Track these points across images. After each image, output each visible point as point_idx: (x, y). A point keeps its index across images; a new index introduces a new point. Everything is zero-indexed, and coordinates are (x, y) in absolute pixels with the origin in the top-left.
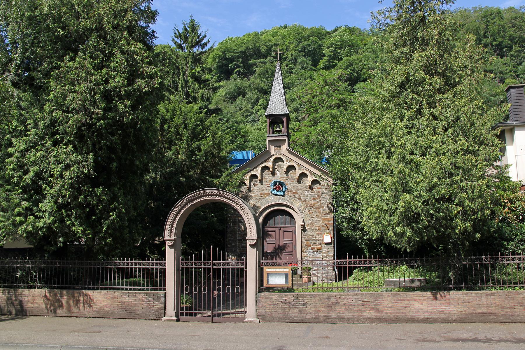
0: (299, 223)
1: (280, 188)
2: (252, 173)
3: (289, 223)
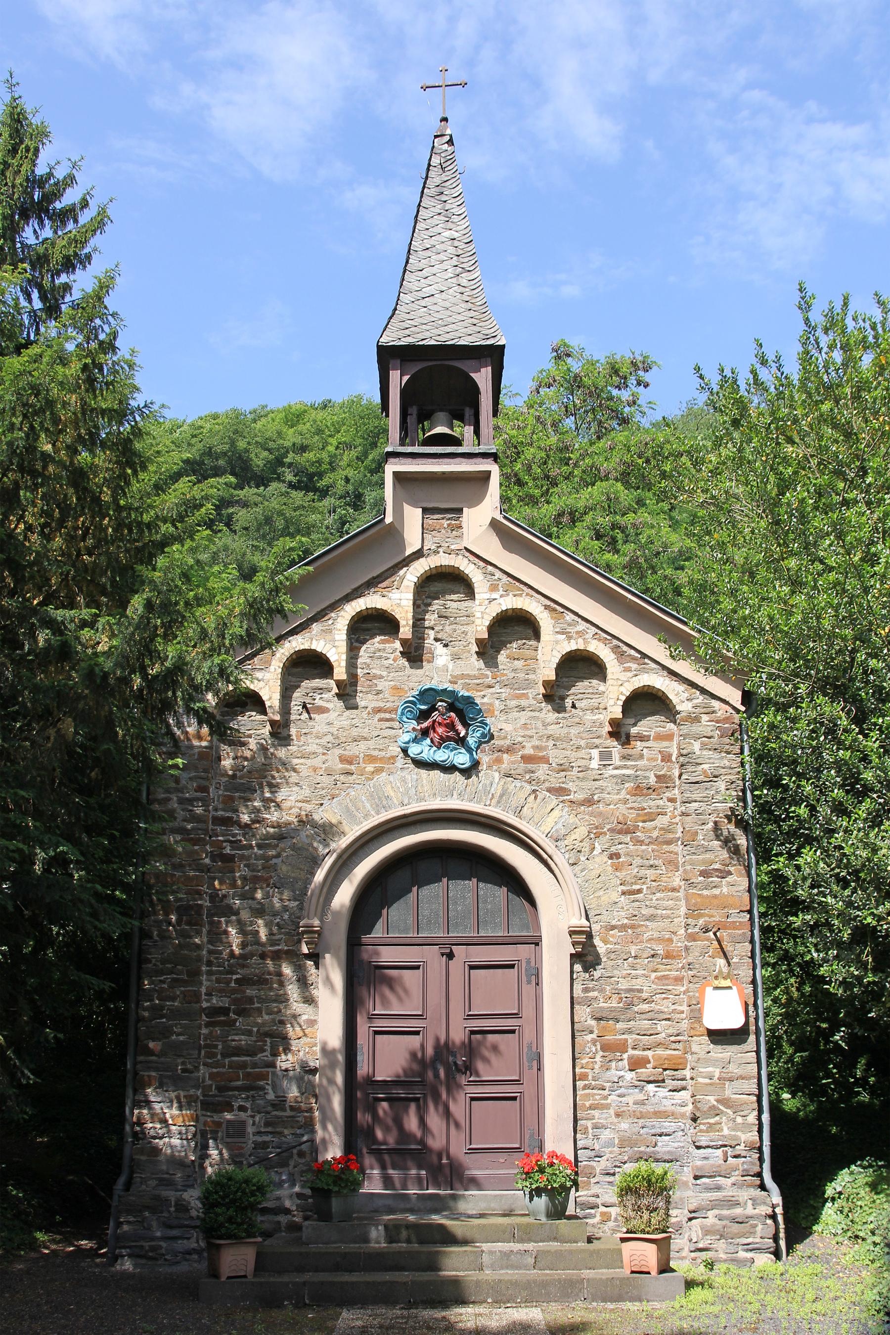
0: (558, 913)
1: (451, 726)
2: (298, 643)
3: (502, 919)
